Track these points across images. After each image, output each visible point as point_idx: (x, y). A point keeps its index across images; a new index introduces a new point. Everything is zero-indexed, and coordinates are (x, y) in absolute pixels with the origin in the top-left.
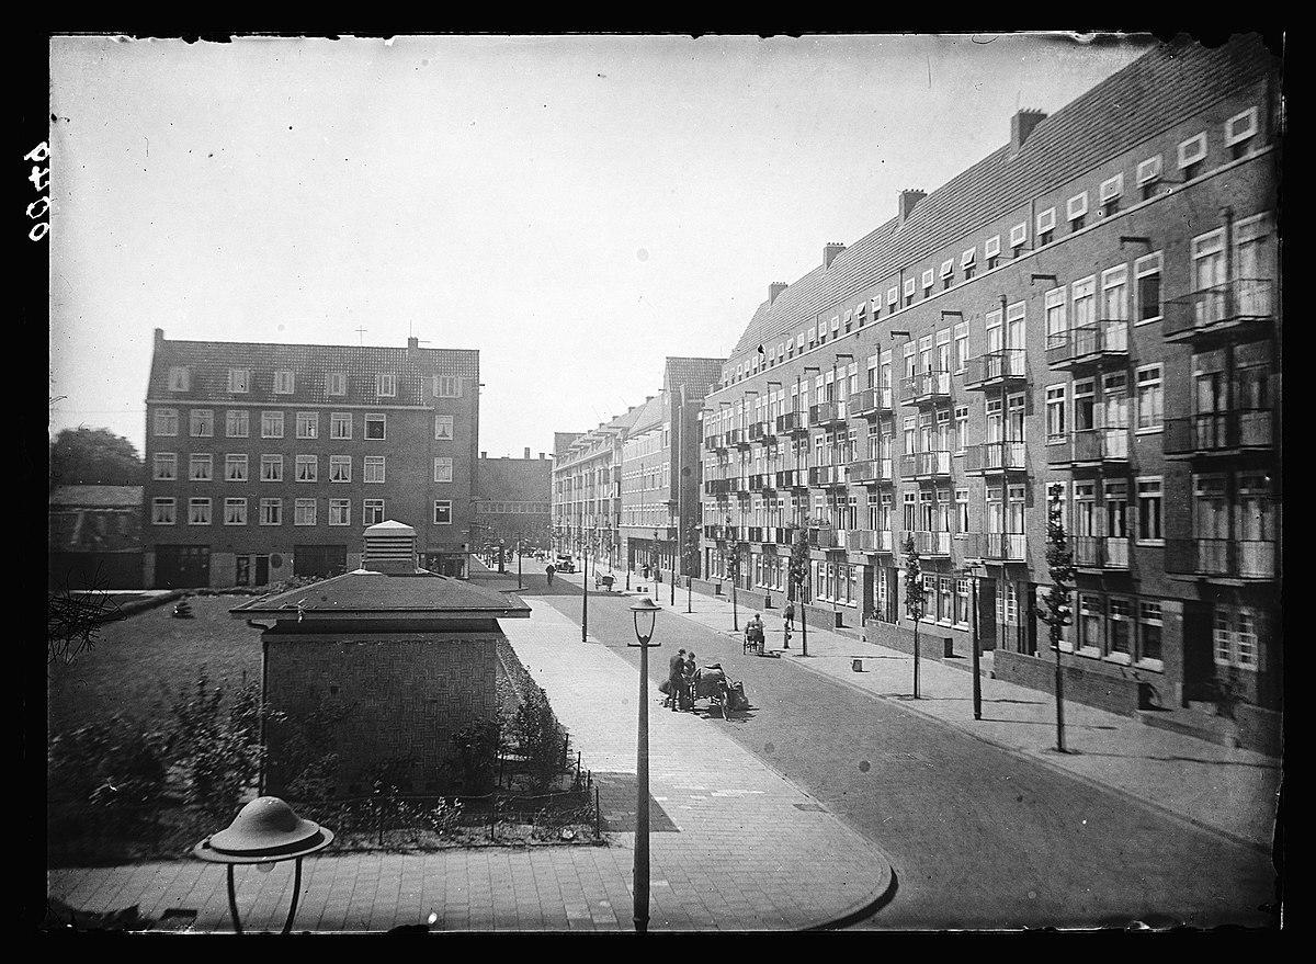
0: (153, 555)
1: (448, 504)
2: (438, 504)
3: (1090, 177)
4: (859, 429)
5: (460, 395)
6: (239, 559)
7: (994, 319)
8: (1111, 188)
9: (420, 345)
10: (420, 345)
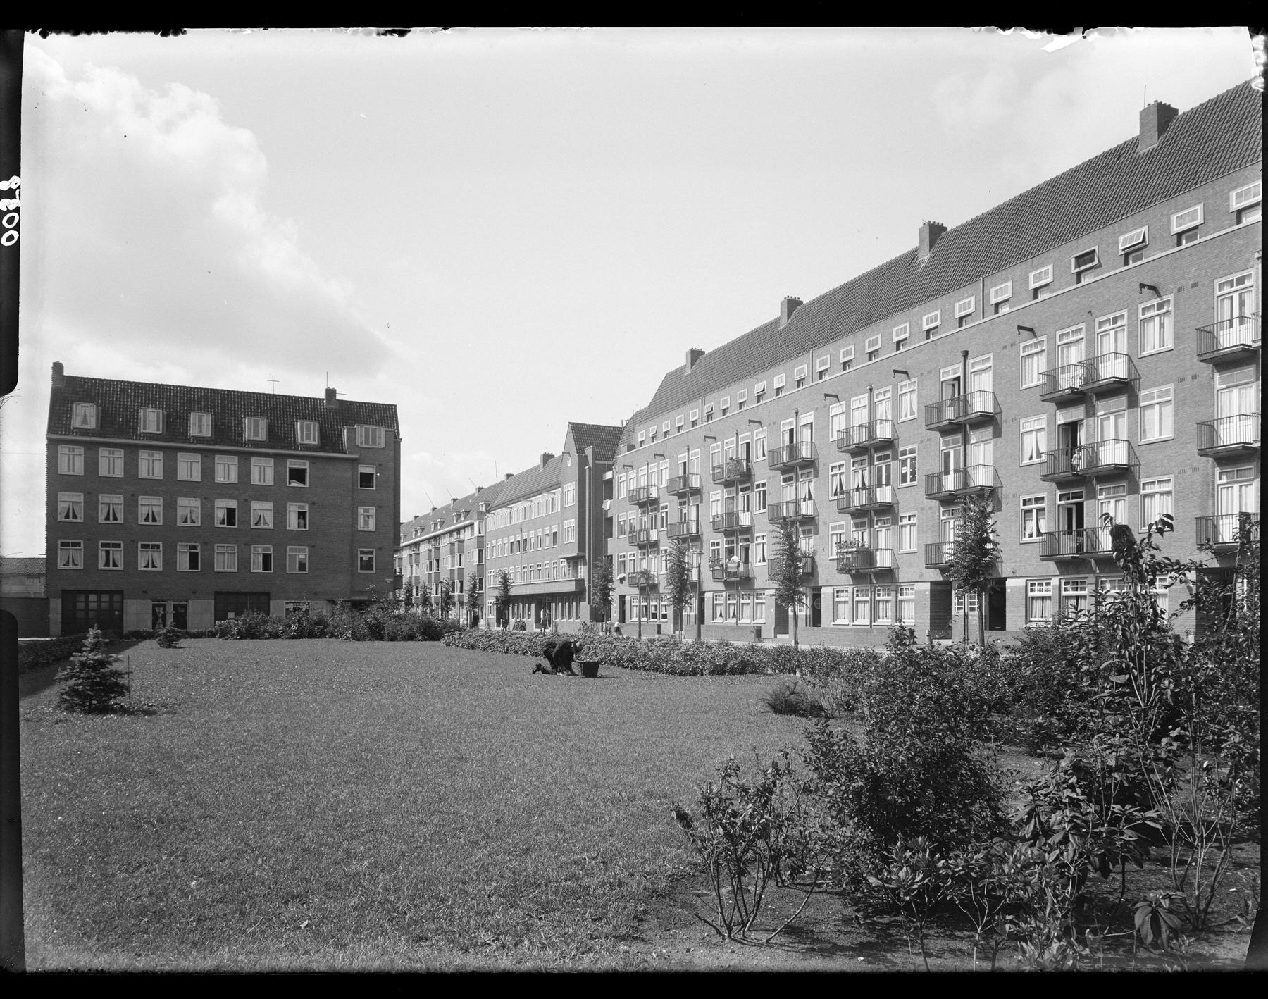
0: (60, 600)
1: (372, 553)
2: (362, 553)
3: (789, 363)
4: (671, 505)
5: (383, 445)
6: (154, 606)
7: (862, 400)
8: (800, 372)
9: (339, 397)
10: (339, 397)
